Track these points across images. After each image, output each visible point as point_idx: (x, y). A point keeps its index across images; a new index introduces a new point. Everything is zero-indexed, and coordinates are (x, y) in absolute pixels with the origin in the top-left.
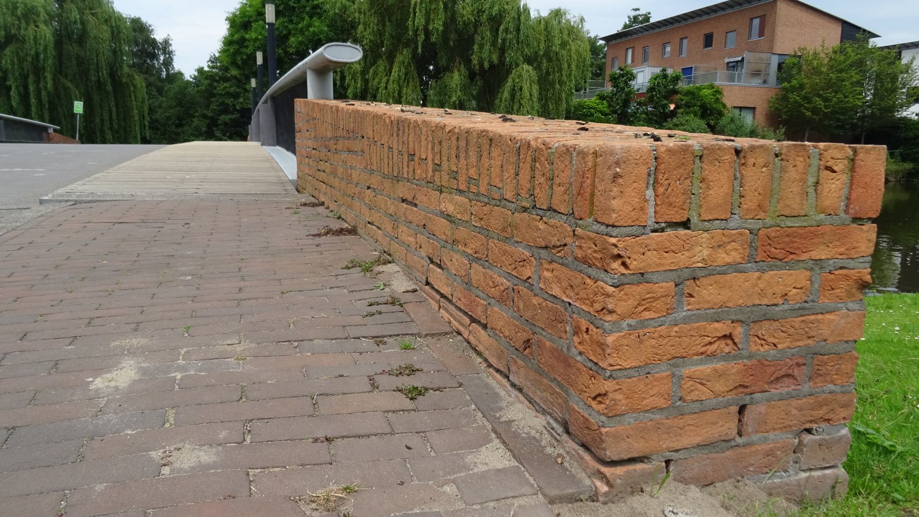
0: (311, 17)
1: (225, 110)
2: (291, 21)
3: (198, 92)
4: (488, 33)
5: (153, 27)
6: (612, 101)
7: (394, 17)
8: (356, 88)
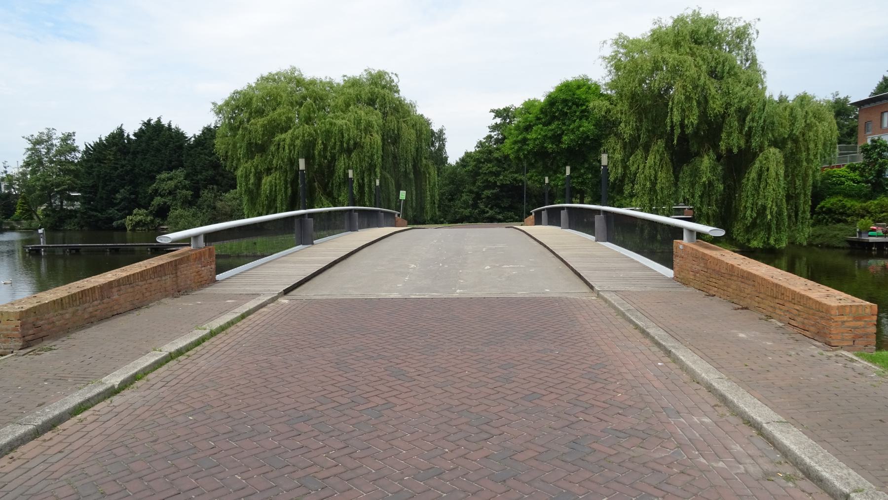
0: (581, 119)
1: (489, 186)
2: (564, 124)
3: (466, 171)
4: (736, 123)
5: (431, 121)
6: (864, 171)
7: (650, 115)
8: (617, 174)
